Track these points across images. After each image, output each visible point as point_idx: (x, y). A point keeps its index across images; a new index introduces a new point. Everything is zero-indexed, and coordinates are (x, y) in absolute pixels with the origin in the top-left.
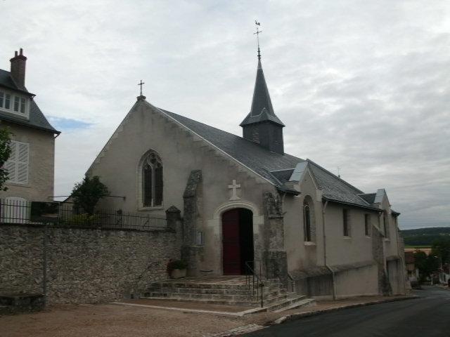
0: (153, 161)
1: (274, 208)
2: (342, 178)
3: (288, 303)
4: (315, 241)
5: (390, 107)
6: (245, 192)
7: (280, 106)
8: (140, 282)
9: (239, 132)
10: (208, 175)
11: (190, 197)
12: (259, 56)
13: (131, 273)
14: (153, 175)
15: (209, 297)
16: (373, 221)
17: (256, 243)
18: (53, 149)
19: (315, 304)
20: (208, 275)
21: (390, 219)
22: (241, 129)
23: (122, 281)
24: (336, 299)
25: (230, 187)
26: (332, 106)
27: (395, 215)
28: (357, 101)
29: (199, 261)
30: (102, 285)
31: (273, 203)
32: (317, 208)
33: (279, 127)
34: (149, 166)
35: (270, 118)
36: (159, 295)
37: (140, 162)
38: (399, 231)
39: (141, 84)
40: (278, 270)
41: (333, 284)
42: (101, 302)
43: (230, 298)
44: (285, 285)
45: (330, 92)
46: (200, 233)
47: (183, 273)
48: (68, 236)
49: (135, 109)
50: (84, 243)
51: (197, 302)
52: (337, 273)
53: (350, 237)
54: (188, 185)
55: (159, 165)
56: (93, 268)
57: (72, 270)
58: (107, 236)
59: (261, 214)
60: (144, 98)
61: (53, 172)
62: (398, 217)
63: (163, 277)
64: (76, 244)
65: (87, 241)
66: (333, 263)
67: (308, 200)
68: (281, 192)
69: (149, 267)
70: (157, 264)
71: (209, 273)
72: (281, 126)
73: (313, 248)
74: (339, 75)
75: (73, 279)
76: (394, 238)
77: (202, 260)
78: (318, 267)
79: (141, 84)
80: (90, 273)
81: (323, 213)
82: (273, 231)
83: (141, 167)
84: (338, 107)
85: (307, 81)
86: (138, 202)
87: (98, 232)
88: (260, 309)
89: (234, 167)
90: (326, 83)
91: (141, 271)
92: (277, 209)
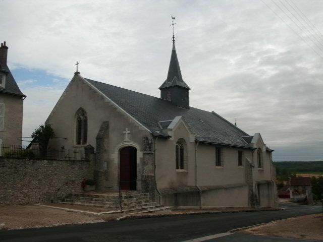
0: (83, 115)
1: (148, 147)
2: (238, 126)
3: (145, 209)
4: (187, 169)
5: (313, 72)
6: (133, 136)
7: (188, 77)
8: (59, 193)
9: (158, 94)
10: (112, 125)
11: (100, 139)
12: (174, 40)
13: (51, 187)
14: (82, 124)
15: (95, 203)
16: (247, 157)
17: (138, 170)
18: (22, 107)
19: (170, 211)
20: (109, 189)
21: (264, 154)
22: (160, 91)
23: (45, 191)
24: (202, 208)
25: (124, 132)
26: (270, 71)
27: (269, 152)
28: (289, 68)
29: (104, 181)
30: (28, 194)
31: (148, 144)
32: (190, 150)
33: (187, 89)
34: (80, 118)
35: (178, 84)
36: (69, 201)
37: (75, 116)
38: (273, 163)
39: (77, 64)
40: (148, 187)
41: (200, 199)
42: (27, 204)
43: (106, 204)
44: (153, 199)
45: (269, 61)
46: (106, 163)
47: (93, 188)
48: (3, 163)
49: (73, 80)
50: (16, 168)
51: (87, 206)
52: (204, 192)
53: (223, 166)
54: (100, 131)
55: (86, 117)
56: (22, 183)
57: (6, 184)
58: (33, 163)
59: (141, 150)
60: (79, 73)
61: (21, 121)
62: (273, 153)
63: (79, 190)
64: (10, 168)
65: (18, 166)
66: (202, 184)
67: (181, 142)
68: (155, 137)
69: (66, 184)
70: (73, 181)
71: (111, 188)
72: (187, 89)
73: (186, 174)
74: (277, 49)
75: (6, 189)
76: (267, 167)
77: (107, 179)
78: (188, 187)
79: (77, 64)
80: (19, 186)
81: (196, 150)
82: (146, 162)
83: (76, 118)
84: (274, 72)
85: (253, 54)
86: (73, 141)
87: (27, 161)
88: (120, 211)
89: (127, 119)
90: (267, 55)
91: (61, 185)
92: (150, 148)
